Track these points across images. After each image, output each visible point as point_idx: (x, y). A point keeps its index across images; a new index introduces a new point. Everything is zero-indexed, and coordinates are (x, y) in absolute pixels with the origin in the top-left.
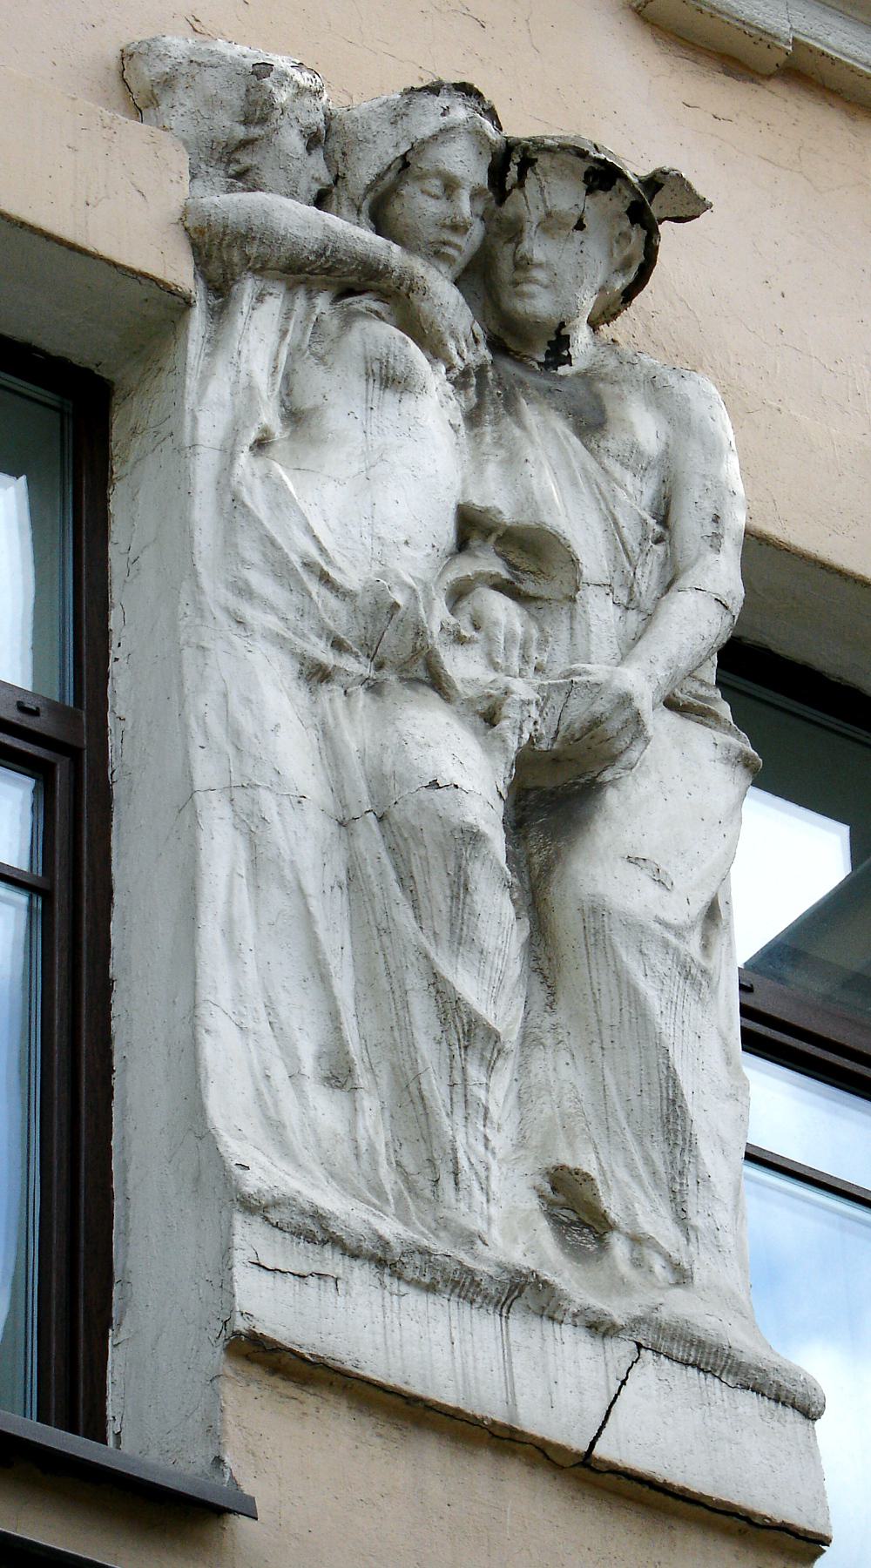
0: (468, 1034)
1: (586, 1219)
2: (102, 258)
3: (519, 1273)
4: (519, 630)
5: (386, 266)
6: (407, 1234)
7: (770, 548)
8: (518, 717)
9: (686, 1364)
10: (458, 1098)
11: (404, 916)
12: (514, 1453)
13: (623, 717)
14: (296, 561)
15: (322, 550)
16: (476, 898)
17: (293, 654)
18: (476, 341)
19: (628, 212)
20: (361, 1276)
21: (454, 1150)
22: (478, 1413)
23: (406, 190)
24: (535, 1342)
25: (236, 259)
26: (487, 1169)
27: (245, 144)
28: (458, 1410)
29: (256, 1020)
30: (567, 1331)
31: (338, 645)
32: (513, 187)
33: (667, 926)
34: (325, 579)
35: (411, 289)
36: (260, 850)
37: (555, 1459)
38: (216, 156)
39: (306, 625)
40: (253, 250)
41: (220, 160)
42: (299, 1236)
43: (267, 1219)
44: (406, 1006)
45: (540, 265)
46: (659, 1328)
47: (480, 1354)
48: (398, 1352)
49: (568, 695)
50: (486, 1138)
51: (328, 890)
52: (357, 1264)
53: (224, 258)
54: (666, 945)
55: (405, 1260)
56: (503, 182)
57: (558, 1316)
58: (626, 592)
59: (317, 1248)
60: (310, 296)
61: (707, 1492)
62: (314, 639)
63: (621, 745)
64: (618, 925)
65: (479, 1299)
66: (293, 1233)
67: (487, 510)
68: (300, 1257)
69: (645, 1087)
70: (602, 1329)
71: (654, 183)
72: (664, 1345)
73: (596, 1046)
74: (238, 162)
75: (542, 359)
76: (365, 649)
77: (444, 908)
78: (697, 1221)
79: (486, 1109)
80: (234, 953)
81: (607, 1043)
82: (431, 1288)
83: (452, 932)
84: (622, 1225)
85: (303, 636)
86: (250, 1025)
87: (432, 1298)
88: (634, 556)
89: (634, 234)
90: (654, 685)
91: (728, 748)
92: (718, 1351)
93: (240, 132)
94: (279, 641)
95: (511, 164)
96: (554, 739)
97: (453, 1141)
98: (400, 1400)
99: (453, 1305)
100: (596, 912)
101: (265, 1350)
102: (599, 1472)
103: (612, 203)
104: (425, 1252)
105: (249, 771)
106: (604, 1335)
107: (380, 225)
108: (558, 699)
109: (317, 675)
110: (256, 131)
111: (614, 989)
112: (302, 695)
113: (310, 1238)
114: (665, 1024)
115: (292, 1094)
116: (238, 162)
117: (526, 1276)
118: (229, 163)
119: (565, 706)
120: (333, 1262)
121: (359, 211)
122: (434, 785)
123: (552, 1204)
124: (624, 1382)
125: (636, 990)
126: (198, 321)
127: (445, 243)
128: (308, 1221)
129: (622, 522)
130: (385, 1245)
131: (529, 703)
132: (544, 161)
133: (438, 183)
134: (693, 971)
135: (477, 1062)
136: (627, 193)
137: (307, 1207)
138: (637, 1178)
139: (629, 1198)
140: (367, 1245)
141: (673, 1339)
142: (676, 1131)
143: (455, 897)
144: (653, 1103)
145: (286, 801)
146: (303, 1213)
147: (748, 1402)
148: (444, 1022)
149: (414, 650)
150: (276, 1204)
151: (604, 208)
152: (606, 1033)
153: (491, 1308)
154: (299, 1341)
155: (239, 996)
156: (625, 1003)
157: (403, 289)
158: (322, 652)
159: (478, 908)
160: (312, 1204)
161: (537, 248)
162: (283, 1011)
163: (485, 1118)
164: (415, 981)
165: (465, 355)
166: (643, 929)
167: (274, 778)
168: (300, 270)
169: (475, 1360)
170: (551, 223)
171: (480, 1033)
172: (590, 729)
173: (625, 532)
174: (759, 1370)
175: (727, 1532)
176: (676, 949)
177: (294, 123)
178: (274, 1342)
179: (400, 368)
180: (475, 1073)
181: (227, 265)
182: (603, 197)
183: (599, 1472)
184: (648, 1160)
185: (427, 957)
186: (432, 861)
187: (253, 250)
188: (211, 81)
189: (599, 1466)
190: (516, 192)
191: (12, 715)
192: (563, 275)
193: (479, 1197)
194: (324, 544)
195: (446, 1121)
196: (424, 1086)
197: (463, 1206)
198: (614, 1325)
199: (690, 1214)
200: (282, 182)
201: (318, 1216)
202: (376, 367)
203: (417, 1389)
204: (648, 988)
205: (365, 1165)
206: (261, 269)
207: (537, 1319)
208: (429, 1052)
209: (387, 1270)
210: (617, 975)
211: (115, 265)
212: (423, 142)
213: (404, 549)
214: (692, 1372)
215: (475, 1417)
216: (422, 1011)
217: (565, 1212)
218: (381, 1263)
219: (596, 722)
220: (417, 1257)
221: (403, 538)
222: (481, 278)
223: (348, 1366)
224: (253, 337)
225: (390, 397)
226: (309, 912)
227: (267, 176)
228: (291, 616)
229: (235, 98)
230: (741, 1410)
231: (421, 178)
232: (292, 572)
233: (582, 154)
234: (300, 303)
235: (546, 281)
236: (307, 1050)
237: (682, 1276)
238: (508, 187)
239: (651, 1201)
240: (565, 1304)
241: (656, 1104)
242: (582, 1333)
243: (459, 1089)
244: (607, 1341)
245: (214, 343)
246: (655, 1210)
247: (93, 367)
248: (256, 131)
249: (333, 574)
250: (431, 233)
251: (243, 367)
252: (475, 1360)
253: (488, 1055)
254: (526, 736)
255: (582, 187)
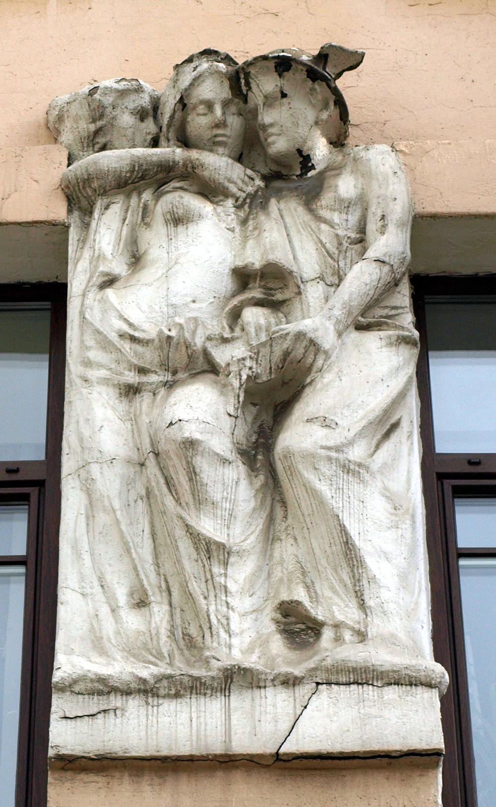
0: (208, 551)
1: (311, 625)
2: (11, 223)
3: (227, 669)
4: (262, 321)
5: (174, 162)
6: (155, 670)
7: (442, 219)
8: (237, 369)
9: (348, 684)
10: (210, 587)
11: (169, 501)
12: (237, 767)
13: (304, 345)
14: (113, 337)
15: (131, 325)
16: (202, 475)
17: (114, 385)
18: (253, 179)
19: (308, 77)
20: (134, 704)
21: (208, 616)
22: (204, 753)
23: (190, 118)
24: (247, 704)
25: (90, 193)
26: (228, 619)
27: (97, 132)
28: (191, 756)
29: (92, 588)
30: (270, 691)
31: (142, 371)
32: (247, 91)
33: (329, 448)
34: (133, 339)
35: (193, 168)
36: (93, 495)
37: (264, 763)
38: (85, 145)
39: (120, 368)
40: (95, 185)
41: (88, 146)
42: (93, 694)
43: (72, 692)
44: (178, 549)
45: (272, 125)
46: (328, 670)
47: (209, 721)
48: (154, 737)
49: (271, 346)
50: (227, 603)
51: (132, 503)
52: (130, 698)
53: (82, 196)
54: (330, 459)
55: (157, 686)
56: (241, 91)
57: (262, 684)
58: (336, 277)
59: (105, 697)
60: (139, 194)
61: (356, 749)
62: (127, 373)
63: (309, 361)
64: (299, 459)
65: (209, 692)
66: (89, 694)
67: (246, 265)
68: (94, 704)
69: (332, 541)
70: (291, 682)
71: (323, 57)
72: (333, 678)
73: (305, 529)
74: (98, 143)
75: (299, 172)
76: (163, 367)
77: (187, 488)
78: (370, 603)
79: (225, 587)
80: (78, 555)
81: (310, 525)
82: (177, 695)
83: (194, 498)
84: (327, 621)
85: (121, 374)
86: (88, 591)
87: (179, 700)
88: (336, 256)
89: (317, 87)
90: (334, 321)
91: (390, 337)
92: (366, 670)
93: (92, 127)
94: (105, 381)
95: (239, 80)
96: (270, 373)
97: (208, 611)
98: (159, 762)
99: (194, 700)
100: (288, 455)
101: (70, 761)
102: (289, 761)
103: (296, 76)
104: (169, 677)
105: (86, 457)
106: (294, 685)
107: (185, 142)
108: (264, 351)
109: (131, 391)
110: (99, 124)
111: (305, 494)
112: (123, 406)
113: (100, 693)
114: (335, 503)
115: (111, 619)
116: (98, 143)
117: (231, 669)
118: (94, 145)
119: (271, 352)
120: (116, 701)
121: (169, 140)
122: (171, 424)
123: (285, 624)
124: (306, 707)
125: (315, 491)
126: (73, 235)
127: (216, 136)
128: (96, 684)
129: (324, 241)
130: (144, 681)
131: (244, 359)
132: (252, 70)
133: (202, 107)
134: (352, 467)
135: (217, 563)
136: (300, 67)
137: (93, 677)
138: (335, 592)
139: (332, 606)
140: (133, 686)
141: (337, 673)
142: (352, 558)
143: (191, 480)
144: (338, 548)
145: (105, 465)
146: (92, 681)
147: (392, 693)
148: (197, 549)
149: (189, 357)
150: (75, 681)
151: (293, 81)
152: (308, 519)
153: (219, 694)
154: (87, 750)
155: (82, 579)
156: (312, 499)
157: (189, 169)
158: (132, 378)
159: (205, 481)
160: (96, 674)
161: (267, 117)
162: (108, 577)
163: (226, 592)
164: (180, 532)
165: (245, 188)
166: (313, 456)
167: (99, 455)
168: (126, 184)
169: (206, 724)
170: (269, 101)
171: (213, 547)
172: (285, 360)
173: (328, 245)
174: (394, 671)
175: (379, 768)
176: (337, 459)
177: (125, 110)
178: (71, 756)
179: (181, 212)
180: (217, 570)
181: (88, 198)
182: (288, 75)
183: (289, 761)
184: (342, 581)
185: (181, 518)
186: (177, 466)
187: (95, 185)
188: (74, 109)
189: (285, 758)
190: (249, 93)
191: (7, 477)
192: (292, 123)
193: (223, 635)
194: (131, 321)
195: (204, 602)
196: (190, 588)
197: (215, 644)
198: (296, 678)
199: (366, 601)
200: (125, 143)
201: (102, 680)
202: (168, 217)
203: (165, 753)
204: (324, 488)
205: (155, 642)
206: (104, 192)
207: (250, 691)
208: (190, 567)
209: (150, 695)
210: (304, 485)
211: (19, 224)
212: (186, 90)
213: (193, 305)
214: (353, 687)
215: (203, 756)
216: (185, 547)
217: (298, 626)
218: (145, 692)
219: (286, 354)
220: (165, 683)
221: (189, 299)
222: (249, 146)
223: (121, 754)
224: (102, 230)
225: (180, 228)
226: (117, 519)
227: (116, 143)
228: (113, 366)
229: (84, 112)
230: (386, 697)
231: (194, 108)
232: (111, 343)
233: (265, 58)
234: (134, 201)
235: (278, 132)
236: (122, 595)
237: (362, 636)
238: (245, 92)
239: (345, 601)
240: (263, 677)
241: (339, 547)
242: (280, 688)
243: (210, 582)
244: (297, 688)
245: (83, 241)
246: (347, 606)
247: (55, 280)
248: (99, 124)
249: (136, 334)
250: (208, 134)
251: (96, 248)
252: (206, 724)
253: (222, 557)
254: (244, 377)
255: (276, 75)
